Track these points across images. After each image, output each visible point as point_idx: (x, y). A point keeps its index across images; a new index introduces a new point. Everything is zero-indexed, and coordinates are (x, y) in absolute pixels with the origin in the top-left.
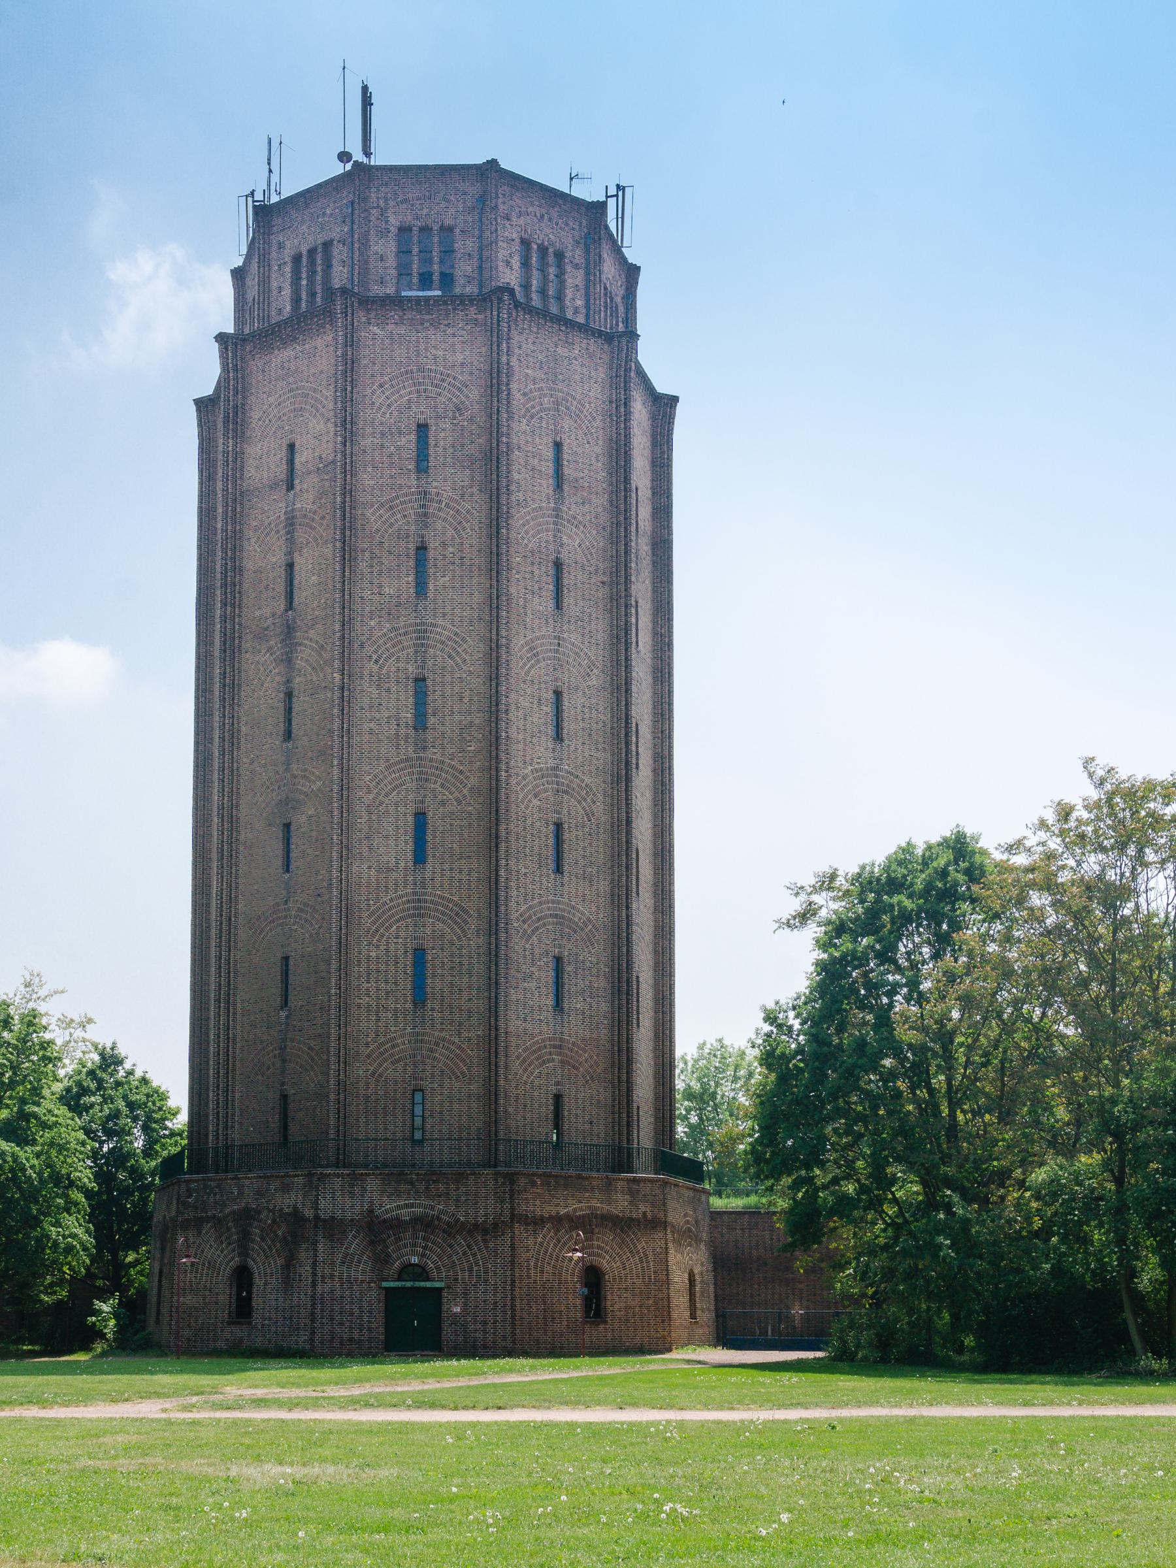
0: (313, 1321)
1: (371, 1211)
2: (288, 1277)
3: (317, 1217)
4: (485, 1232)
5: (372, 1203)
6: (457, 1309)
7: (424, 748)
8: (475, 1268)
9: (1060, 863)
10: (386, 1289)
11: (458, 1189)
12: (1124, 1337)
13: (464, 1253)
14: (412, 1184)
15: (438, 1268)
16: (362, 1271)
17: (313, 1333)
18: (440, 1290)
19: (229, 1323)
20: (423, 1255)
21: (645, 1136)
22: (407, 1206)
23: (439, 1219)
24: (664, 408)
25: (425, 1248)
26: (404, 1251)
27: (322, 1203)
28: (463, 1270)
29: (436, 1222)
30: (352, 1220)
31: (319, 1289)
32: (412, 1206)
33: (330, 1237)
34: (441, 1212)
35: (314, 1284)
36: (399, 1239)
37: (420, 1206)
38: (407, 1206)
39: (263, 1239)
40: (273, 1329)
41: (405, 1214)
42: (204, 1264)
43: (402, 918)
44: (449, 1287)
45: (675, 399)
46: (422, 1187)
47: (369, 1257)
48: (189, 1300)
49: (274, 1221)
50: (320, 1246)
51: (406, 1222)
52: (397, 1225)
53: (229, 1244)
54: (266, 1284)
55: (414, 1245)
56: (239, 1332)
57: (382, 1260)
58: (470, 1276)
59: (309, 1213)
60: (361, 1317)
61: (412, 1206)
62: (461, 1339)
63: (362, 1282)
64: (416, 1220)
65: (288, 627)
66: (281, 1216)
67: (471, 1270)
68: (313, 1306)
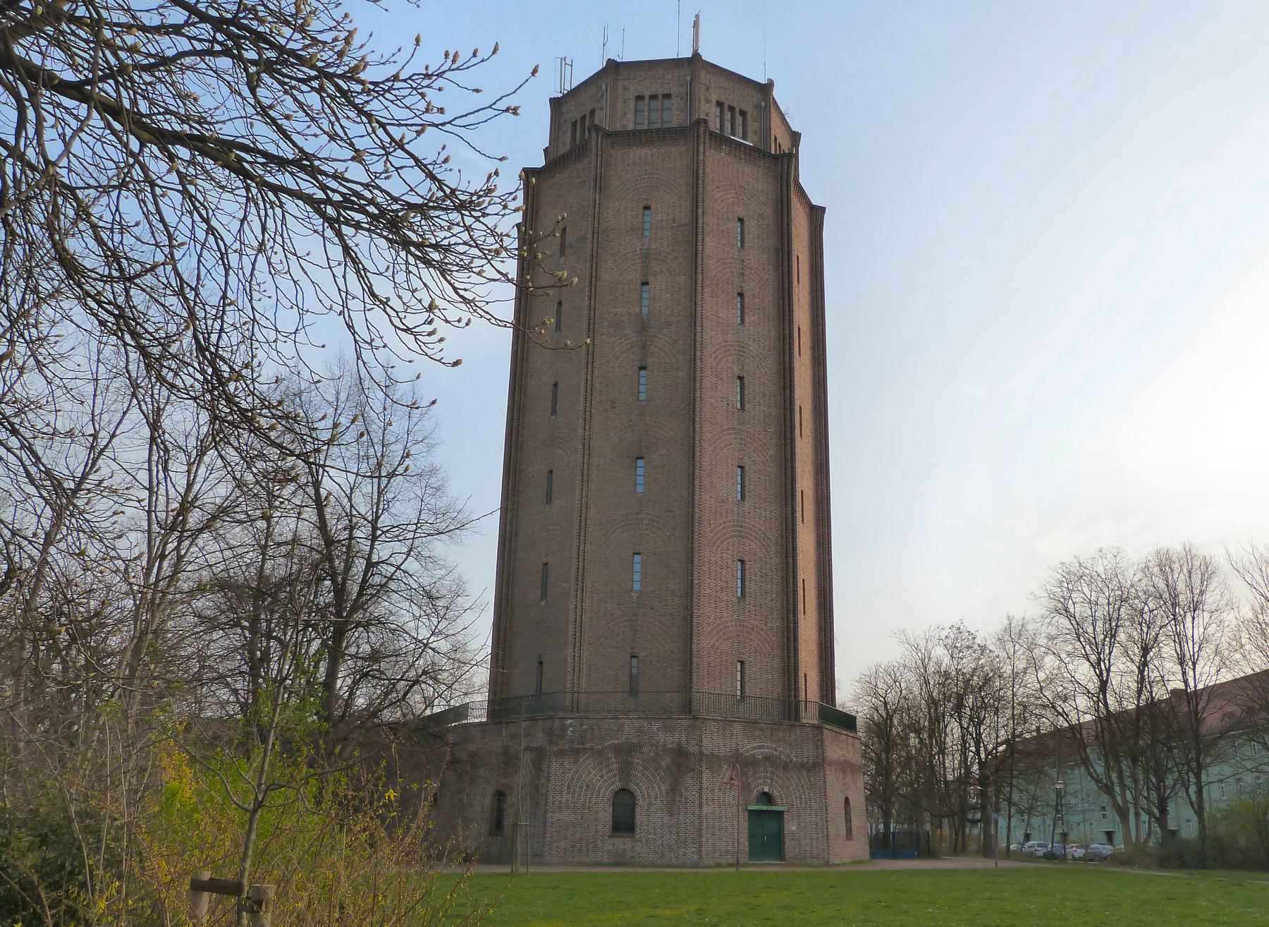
0: (700, 836)
1: (737, 750)
2: (673, 800)
3: (701, 753)
4: (808, 770)
6: (794, 828)
7: (744, 424)
14: (762, 730)
16: (731, 796)
17: (700, 846)
18: (782, 812)
19: (610, 837)
21: (810, 689)
22: (760, 747)
24: (816, 215)
27: (705, 742)
31: (704, 810)
32: (762, 747)
33: (711, 769)
34: (781, 753)
35: (700, 805)
36: (755, 773)
38: (760, 747)
39: (645, 768)
40: (659, 842)
41: (759, 754)
42: (581, 787)
43: (731, 537)
45: (823, 209)
46: (768, 734)
48: (566, 816)
49: (656, 754)
50: (705, 776)
53: (610, 771)
54: (650, 804)
56: (622, 843)
57: (746, 788)
59: (693, 749)
64: (766, 758)
65: (643, 323)
66: (664, 750)
68: (700, 823)
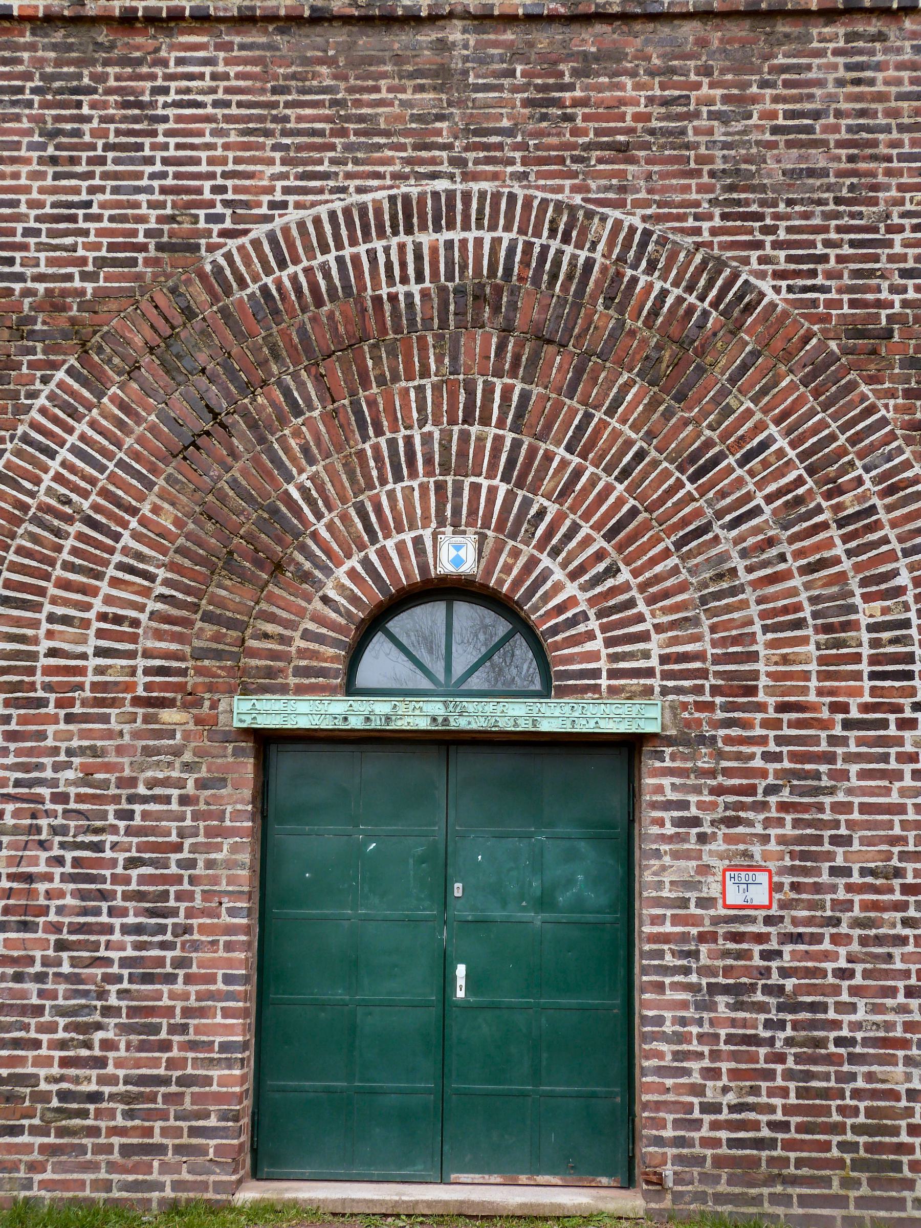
5: (186, 196)
8: (867, 613)
9: (907, 417)
10: (266, 742)
11: (741, 103)
12: (320, 581)
13: (794, 507)
14: (442, 77)
15: (612, 608)
18: (630, 747)
20: (515, 523)
22: (408, 215)
23: (617, 292)
25: (522, 472)
26: (391, 492)
28: (783, 621)
29: (603, 317)
30: (54, 304)
32: (444, 213)
37: (493, 211)
38: (408, 215)
41: (401, 269)
44: (688, 739)
47: (155, 536)
51: (405, 318)
52: (347, 340)
55: (455, 460)
58: (834, 665)
60: (81, 937)
61: (444, 213)
62: (778, 1101)
63: (106, 696)
67: (837, 626)
